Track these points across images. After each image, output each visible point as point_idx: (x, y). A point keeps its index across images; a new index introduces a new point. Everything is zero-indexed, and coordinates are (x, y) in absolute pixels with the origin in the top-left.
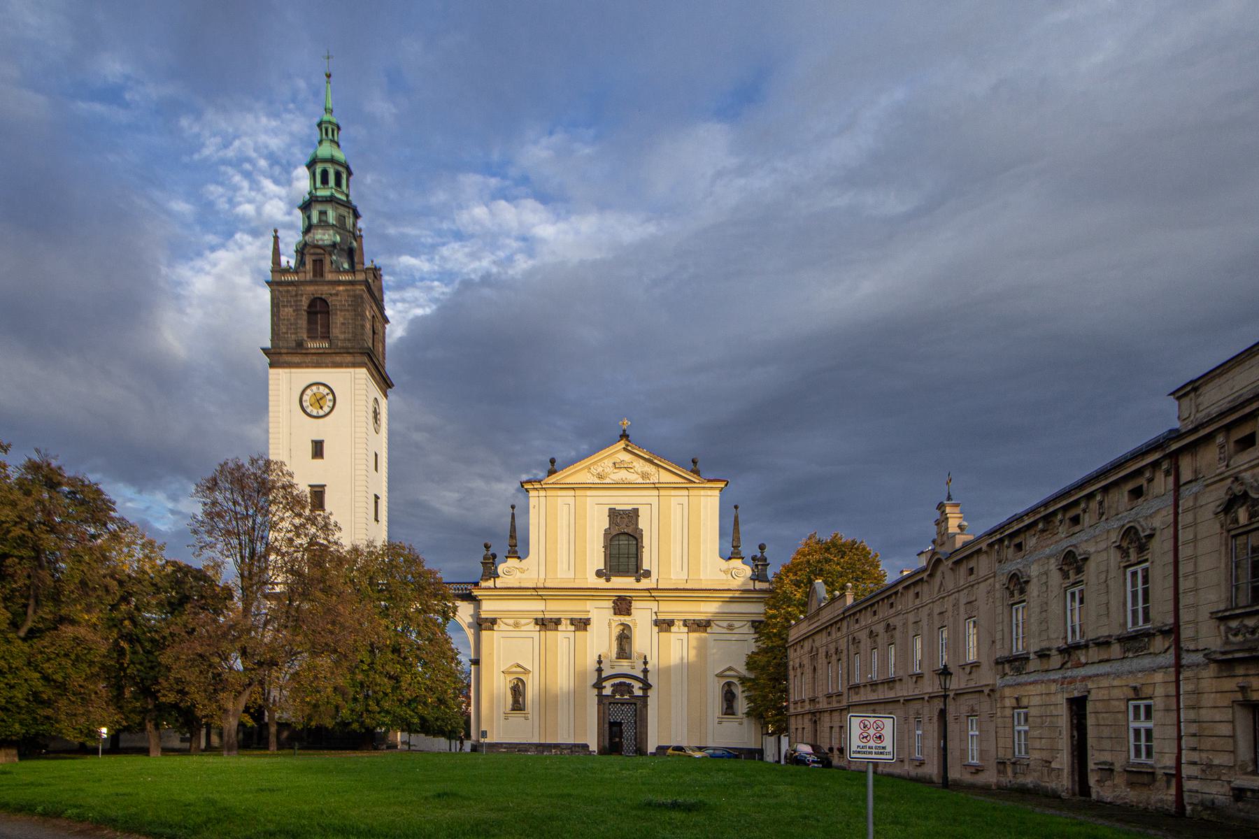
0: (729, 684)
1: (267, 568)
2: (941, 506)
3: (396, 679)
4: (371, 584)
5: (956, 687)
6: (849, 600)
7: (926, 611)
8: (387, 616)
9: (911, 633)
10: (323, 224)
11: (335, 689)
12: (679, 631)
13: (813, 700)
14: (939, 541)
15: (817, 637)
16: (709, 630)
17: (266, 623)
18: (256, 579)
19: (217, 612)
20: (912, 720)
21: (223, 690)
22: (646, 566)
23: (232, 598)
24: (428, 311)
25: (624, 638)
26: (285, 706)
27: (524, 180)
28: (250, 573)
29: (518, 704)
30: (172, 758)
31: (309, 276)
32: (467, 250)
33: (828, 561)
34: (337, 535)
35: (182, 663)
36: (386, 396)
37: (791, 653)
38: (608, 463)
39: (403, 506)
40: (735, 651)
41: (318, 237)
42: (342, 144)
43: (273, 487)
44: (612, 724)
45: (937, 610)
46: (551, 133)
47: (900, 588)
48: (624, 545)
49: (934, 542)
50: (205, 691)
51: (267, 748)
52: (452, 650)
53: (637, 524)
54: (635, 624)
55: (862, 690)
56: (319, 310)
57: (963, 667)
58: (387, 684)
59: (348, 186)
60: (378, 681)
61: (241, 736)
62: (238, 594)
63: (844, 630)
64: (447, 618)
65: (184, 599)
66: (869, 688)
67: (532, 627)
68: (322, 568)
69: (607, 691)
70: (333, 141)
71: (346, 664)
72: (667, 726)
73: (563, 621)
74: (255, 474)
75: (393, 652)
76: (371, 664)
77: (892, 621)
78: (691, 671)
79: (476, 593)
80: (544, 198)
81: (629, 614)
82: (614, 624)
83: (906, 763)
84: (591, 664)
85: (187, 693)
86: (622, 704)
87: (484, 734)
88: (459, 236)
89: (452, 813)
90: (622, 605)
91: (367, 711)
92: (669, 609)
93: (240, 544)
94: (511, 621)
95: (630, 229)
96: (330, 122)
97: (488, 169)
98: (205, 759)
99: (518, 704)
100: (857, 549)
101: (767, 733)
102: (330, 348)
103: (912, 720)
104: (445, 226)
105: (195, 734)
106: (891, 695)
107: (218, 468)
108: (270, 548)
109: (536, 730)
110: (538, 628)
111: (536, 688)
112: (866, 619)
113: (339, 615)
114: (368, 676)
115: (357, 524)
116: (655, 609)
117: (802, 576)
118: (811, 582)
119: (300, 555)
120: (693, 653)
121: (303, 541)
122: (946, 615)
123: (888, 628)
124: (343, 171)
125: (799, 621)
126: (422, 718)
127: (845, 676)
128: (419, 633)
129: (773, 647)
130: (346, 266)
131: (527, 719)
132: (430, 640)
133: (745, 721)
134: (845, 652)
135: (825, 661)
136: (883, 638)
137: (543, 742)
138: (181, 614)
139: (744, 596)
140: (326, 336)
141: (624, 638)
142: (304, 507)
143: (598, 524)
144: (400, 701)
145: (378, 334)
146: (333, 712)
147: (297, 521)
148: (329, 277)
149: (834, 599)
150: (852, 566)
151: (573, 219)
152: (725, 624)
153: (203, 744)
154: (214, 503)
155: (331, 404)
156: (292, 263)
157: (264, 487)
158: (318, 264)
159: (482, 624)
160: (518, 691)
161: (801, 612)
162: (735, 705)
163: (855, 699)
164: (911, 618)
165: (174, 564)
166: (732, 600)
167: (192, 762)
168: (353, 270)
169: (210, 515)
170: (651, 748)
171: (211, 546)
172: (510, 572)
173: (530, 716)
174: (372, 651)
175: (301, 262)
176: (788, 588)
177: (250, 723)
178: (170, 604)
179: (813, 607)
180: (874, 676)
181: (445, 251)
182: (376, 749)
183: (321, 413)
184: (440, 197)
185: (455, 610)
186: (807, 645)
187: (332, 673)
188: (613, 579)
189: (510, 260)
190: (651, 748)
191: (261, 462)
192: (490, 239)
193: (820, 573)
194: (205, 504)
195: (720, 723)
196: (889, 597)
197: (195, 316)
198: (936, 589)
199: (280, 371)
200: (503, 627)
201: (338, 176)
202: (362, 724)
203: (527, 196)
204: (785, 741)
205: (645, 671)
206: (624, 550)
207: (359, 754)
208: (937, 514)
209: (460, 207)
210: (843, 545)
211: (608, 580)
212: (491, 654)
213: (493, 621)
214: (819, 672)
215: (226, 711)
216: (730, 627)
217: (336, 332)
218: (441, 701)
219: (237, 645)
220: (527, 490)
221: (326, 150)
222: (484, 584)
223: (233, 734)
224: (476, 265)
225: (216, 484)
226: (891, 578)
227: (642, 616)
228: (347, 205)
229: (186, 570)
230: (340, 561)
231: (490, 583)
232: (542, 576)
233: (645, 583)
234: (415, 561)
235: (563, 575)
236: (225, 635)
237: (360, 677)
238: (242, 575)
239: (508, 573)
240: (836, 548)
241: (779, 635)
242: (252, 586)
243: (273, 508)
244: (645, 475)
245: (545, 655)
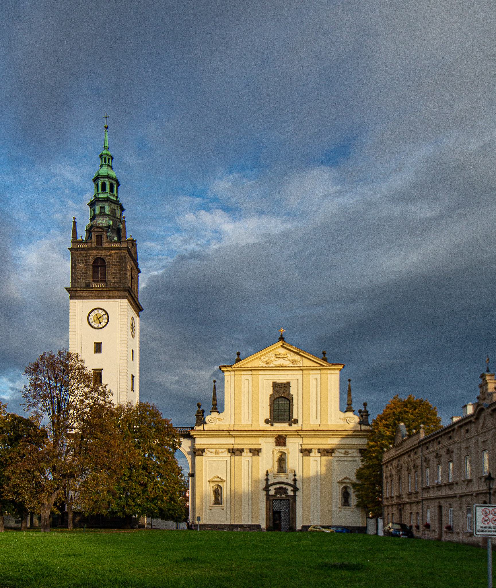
0: (346, 488)
1: (68, 418)
2: (483, 376)
3: (144, 485)
4: (129, 428)
5: (477, 489)
6: (422, 435)
7: (473, 441)
8: (139, 448)
9: (464, 454)
10: (103, 214)
11: (108, 492)
12: (315, 454)
13: (399, 497)
14: (482, 397)
15: (402, 458)
16: (333, 455)
17: (67, 451)
18: (61, 425)
19: (38, 445)
20: (464, 508)
21: (41, 492)
22: (295, 417)
23: (47, 437)
24: (160, 272)
25: (282, 460)
26: (77, 502)
27: (215, 199)
28: (58, 421)
29: (218, 501)
30: (11, 533)
31: (94, 245)
32: (181, 238)
33: (406, 412)
34: (111, 398)
35: (17, 476)
36: (139, 316)
37: (384, 468)
38: (272, 354)
39: (147, 385)
40: (350, 467)
41: (100, 222)
42: (113, 167)
43: (72, 369)
44: (275, 513)
45: (481, 439)
46: (230, 173)
47: (456, 427)
48: (281, 403)
49: (478, 398)
50: (31, 492)
51: (67, 527)
52: (178, 468)
53: (289, 391)
54: (288, 452)
55: (431, 490)
56: (99, 265)
57: (464, 481)
58: (139, 489)
59: (117, 192)
60: (134, 486)
61: (51, 519)
62: (50, 434)
63: (419, 453)
64: (175, 449)
65: (19, 437)
66: (436, 489)
67: (226, 454)
68: (101, 419)
69: (272, 493)
70: (108, 165)
71: (115, 476)
72: (309, 513)
73: (245, 450)
74: (61, 361)
75: (143, 469)
76: (130, 477)
77: (451, 447)
78: (322, 480)
79: (192, 433)
80: (227, 209)
81: (285, 445)
82: (276, 452)
83: (461, 535)
84: (262, 475)
85: (20, 494)
86: (281, 500)
87: (199, 519)
88: (179, 230)
89: (195, 572)
90: (281, 441)
91: (127, 504)
92: (309, 442)
93: (52, 403)
94: (214, 451)
95: (275, 226)
96: (107, 155)
97: (194, 194)
98: (31, 534)
99: (218, 501)
100: (423, 405)
101: (369, 517)
102: (106, 287)
103: (464, 508)
104: (170, 225)
105: (24, 518)
106: (450, 493)
107: (40, 358)
108: (71, 406)
109: (229, 516)
110: (230, 454)
111: (229, 491)
112: (434, 447)
113: (112, 446)
114: (128, 484)
115: (122, 392)
116: (301, 443)
117: (390, 421)
118: (395, 425)
119: (88, 410)
120: (324, 469)
121: (90, 401)
122: (487, 443)
123: (449, 452)
124: (115, 183)
125: (389, 449)
126: (160, 509)
127: (420, 482)
128: (158, 458)
129: (373, 465)
130: (116, 239)
131: (223, 509)
132: (165, 462)
133: (356, 510)
134: (420, 467)
135: (407, 473)
136: (444, 458)
137: (233, 523)
138: (16, 446)
139: (355, 434)
140: (103, 280)
141: (282, 460)
142: (90, 381)
143: (266, 392)
144: (147, 499)
145: (134, 280)
146: (106, 506)
147: (86, 390)
148: (106, 245)
149: (410, 436)
150: (420, 415)
151: (243, 220)
152: (343, 451)
153: (29, 525)
154: (37, 379)
155: (106, 321)
156: (84, 238)
157: (67, 369)
158: (99, 238)
159: (196, 452)
160: (218, 493)
161: (390, 443)
162: (349, 500)
163: (427, 495)
164: (464, 445)
165: (13, 416)
166: (347, 437)
167: (24, 536)
168: (119, 241)
169: (34, 386)
170: (299, 527)
171: (36, 405)
172: (213, 421)
173: (225, 508)
174: (130, 469)
175: (89, 237)
176: (382, 428)
177: (57, 512)
178: (10, 440)
179: (399, 440)
180: (440, 481)
181: (169, 239)
182: (132, 528)
183: (100, 326)
184: (167, 209)
185: (180, 444)
186: (395, 463)
187: (107, 482)
188: (276, 425)
189: (208, 243)
190: (299, 527)
191: (65, 354)
192: (197, 232)
193: (400, 420)
194: (31, 380)
195: (340, 511)
196: (448, 433)
197: (26, 278)
198: (480, 427)
199: (76, 301)
200: (209, 454)
201: (112, 186)
202: (124, 513)
203: (217, 208)
204: (380, 522)
205: (295, 480)
206: (281, 407)
207: (122, 531)
208: (480, 381)
209: (178, 215)
210: (415, 402)
211: (272, 425)
212: (202, 470)
213: (203, 451)
214: (403, 479)
215: (43, 505)
216: (346, 453)
217: (109, 277)
218: (171, 499)
219: (51, 465)
220: (223, 372)
221: (105, 171)
222: (197, 428)
223: (47, 518)
224: (187, 246)
225: (38, 367)
226: (445, 423)
227: (292, 447)
228: (117, 203)
229: (20, 420)
230: (112, 414)
231: (201, 428)
232: (232, 423)
233: (294, 427)
234: (156, 414)
235: (245, 422)
236: (43, 458)
237: (123, 484)
238: (53, 422)
239: (212, 421)
240: (410, 404)
241: (376, 457)
242: (59, 429)
243: (72, 382)
244: (294, 362)
245: (234, 471)
